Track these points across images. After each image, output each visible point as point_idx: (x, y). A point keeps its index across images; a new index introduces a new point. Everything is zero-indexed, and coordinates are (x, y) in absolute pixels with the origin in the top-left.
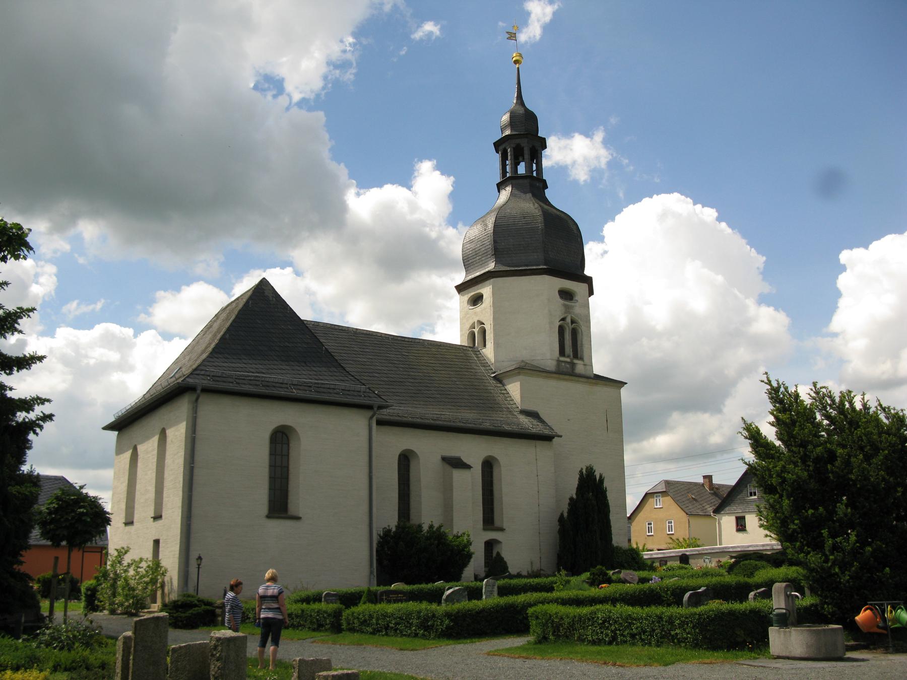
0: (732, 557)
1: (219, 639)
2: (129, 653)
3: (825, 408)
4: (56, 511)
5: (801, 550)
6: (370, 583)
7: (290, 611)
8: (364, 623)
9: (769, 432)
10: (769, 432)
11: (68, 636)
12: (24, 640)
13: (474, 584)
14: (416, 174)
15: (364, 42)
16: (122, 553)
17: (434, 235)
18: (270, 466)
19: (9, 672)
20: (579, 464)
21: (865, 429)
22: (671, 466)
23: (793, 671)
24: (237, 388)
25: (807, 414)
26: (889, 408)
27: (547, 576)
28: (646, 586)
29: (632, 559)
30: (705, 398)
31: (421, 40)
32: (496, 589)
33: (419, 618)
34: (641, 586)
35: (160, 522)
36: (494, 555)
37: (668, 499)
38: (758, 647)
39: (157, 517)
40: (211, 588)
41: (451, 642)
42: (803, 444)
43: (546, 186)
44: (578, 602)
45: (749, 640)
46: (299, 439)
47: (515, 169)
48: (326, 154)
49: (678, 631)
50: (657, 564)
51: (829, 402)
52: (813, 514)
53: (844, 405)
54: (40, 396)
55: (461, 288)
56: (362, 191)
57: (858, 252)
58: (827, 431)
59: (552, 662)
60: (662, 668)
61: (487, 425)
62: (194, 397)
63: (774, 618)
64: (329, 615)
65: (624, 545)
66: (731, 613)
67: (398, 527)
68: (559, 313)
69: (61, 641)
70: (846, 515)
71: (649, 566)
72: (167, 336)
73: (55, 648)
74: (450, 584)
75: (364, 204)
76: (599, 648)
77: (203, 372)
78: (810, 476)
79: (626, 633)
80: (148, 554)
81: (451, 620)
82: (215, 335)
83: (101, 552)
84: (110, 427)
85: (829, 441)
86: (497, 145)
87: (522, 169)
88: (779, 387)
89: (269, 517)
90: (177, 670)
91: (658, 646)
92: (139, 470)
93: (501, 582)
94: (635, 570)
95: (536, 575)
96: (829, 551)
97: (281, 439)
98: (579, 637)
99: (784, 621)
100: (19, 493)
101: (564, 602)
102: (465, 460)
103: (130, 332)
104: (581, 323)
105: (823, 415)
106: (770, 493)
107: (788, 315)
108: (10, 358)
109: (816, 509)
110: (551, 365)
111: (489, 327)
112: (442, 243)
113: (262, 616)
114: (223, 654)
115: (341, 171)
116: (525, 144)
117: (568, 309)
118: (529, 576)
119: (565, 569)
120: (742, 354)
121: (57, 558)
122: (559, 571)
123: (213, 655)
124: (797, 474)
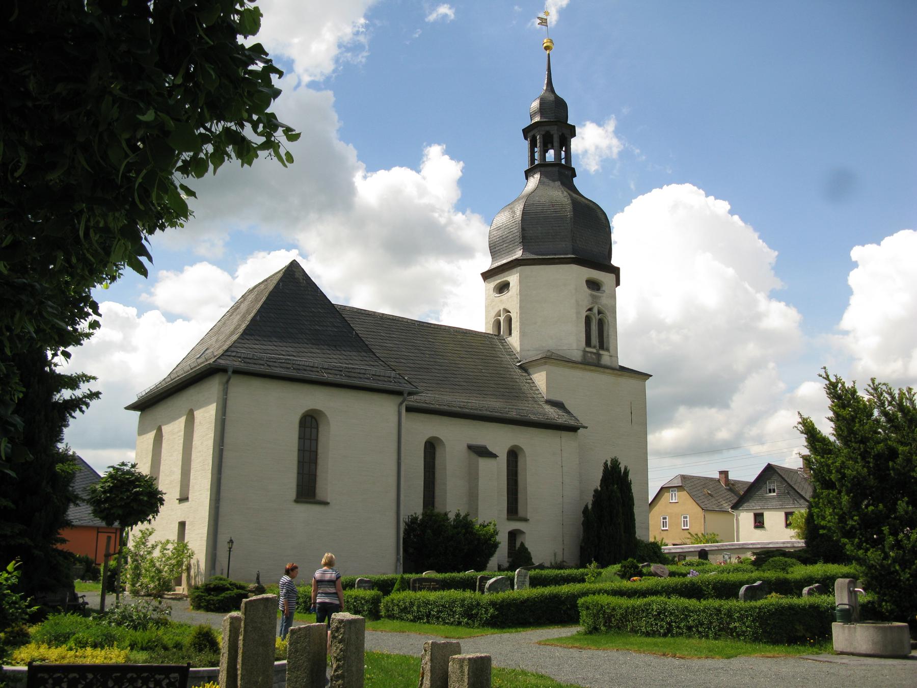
1: (341, 621)
3: (883, 404)
4: (111, 490)
5: (859, 547)
8: (405, 610)
9: (827, 429)
10: (827, 429)
11: (140, 617)
14: (425, 159)
15: (378, 23)
17: (443, 221)
19: (89, 649)
23: (864, 668)
24: (268, 370)
29: (654, 553)
30: (711, 393)
31: (435, 22)
32: (528, 579)
33: (462, 606)
35: (185, 505)
36: (518, 545)
37: (684, 495)
38: (819, 643)
39: (183, 499)
40: (241, 573)
42: (864, 441)
43: (574, 175)
45: (808, 635)
46: (328, 423)
48: (333, 135)
49: (737, 624)
55: (487, 276)
56: (369, 174)
57: (870, 248)
60: (726, 661)
61: (513, 414)
62: (225, 379)
63: (838, 614)
64: (367, 602)
66: (791, 608)
67: (424, 514)
68: (586, 304)
69: (133, 621)
70: (907, 512)
75: (372, 188)
77: (234, 354)
79: (682, 624)
80: (173, 536)
81: (496, 609)
82: (244, 317)
84: (133, 407)
86: (526, 132)
87: (551, 155)
88: (837, 383)
89: (297, 501)
90: (296, 651)
91: (716, 639)
92: (164, 451)
93: (532, 573)
95: (560, 567)
97: (310, 424)
99: (848, 617)
100: (63, 471)
102: (490, 449)
103: (132, 311)
104: (608, 314)
106: (827, 488)
107: (799, 312)
109: (877, 506)
110: (577, 355)
112: (450, 229)
114: (346, 636)
115: (350, 152)
116: (555, 131)
117: (595, 299)
118: (552, 567)
119: (596, 560)
120: (752, 350)
124: (857, 470)
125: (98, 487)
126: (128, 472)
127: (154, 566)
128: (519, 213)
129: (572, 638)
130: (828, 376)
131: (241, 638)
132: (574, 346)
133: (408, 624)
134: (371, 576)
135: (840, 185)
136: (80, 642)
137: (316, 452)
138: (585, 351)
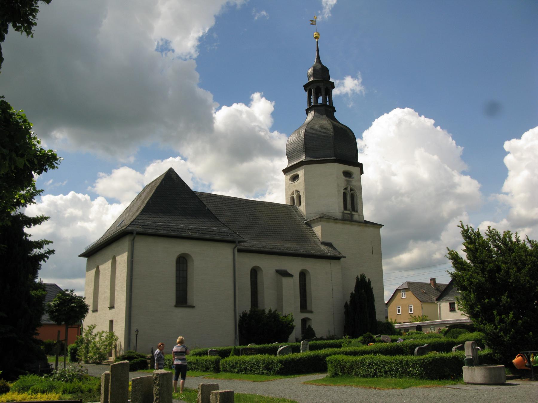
0: (447, 327)
1: (158, 374)
2: (108, 382)
4: (58, 305)
5: (482, 322)
6: (235, 344)
7: (189, 361)
8: (233, 367)
9: (463, 256)
10: (463, 256)
11: (70, 375)
12: (45, 377)
13: (295, 344)
16: (91, 328)
18: (177, 277)
19: (39, 394)
20: (356, 273)
21: (517, 253)
22: (412, 273)
25: (484, 245)
26: (533, 241)
27: (338, 339)
28: (395, 343)
29: (388, 328)
30: (428, 232)
32: (308, 346)
33: (264, 363)
34: (392, 344)
35: (113, 310)
37: (409, 293)
39: (112, 307)
40: (142, 350)
41: (283, 377)
42: (482, 262)
44: (355, 353)
47: (316, 101)
49: (411, 369)
50: (403, 331)
51: (497, 238)
52: (488, 302)
53: (506, 240)
54: (46, 239)
55: (285, 171)
58: (497, 254)
59: (340, 387)
60: (402, 390)
61: (302, 251)
62: (132, 238)
63: (466, 361)
65: (383, 320)
66: (442, 359)
67: (251, 311)
68: (343, 185)
69: (66, 378)
70: (507, 302)
71: (398, 332)
72: (111, 201)
73: (63, 381)
74: (282, 344)
75: (222, 116)
76: (367, 379)
77: (137, 223)
78: (486, 281)
80: (107, 329)
81: (283, 365)
82: (143, 202)
83: (78, 328)
85: (497, 260)
86: (306, 87)
87: (320, 101)
88: (468, 229)
90: (135, 391)
91: (400, 378)
93: (311, 343)
94: (389, 335)
96: (498, 323)
97: (182, 262)
98: (355, 374)
99: (471, 363)
100: (36, 295)
101: (347, 354)
103: (87, 197)
104: (356, 191)
105: (493, 245)
107: (479, 182)
108: (29, 218)
110: (339, 215)
111: (302, 194)
113: (175, 363)
114: (161, 382)
115: (209, 97)
116: (322, 86)
117: (348, 182)
120: (450, 205)
121: (59, 332)
122: (345, 336)
123: (155, 383)
125: (52, 304)
126: (68, 295)
127: (96, 346)
128: (302, 135)
129: (323, 380)
130: (463, 226)
131: (110, 385)
132: (337, 210)
133: (234, 374)
134: (217, 348)
135: (493, 109)
136: (35, 390)
137: (187, 277)
138: (343, 213)
